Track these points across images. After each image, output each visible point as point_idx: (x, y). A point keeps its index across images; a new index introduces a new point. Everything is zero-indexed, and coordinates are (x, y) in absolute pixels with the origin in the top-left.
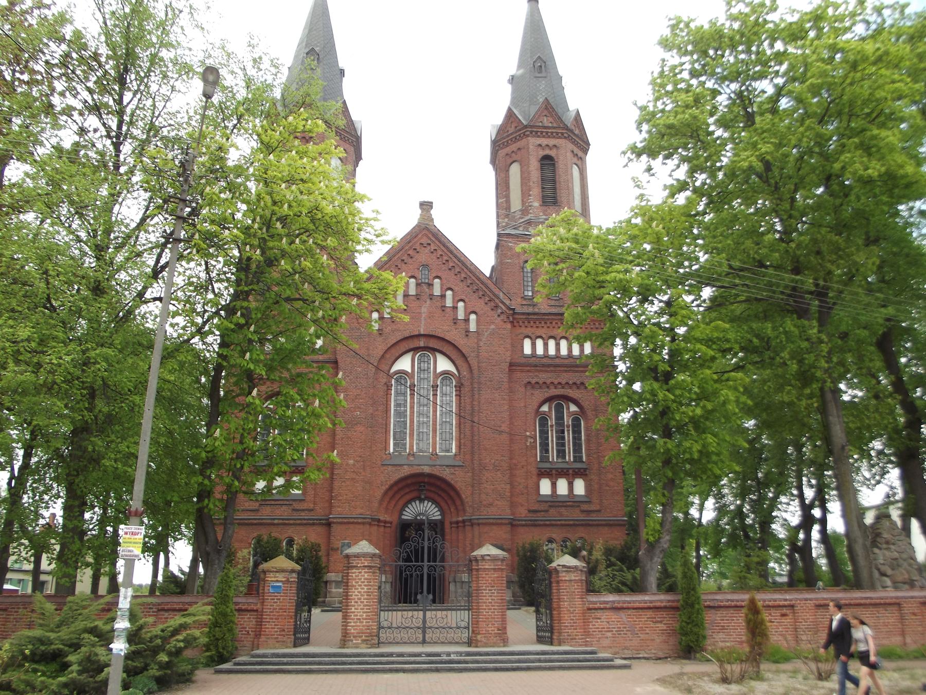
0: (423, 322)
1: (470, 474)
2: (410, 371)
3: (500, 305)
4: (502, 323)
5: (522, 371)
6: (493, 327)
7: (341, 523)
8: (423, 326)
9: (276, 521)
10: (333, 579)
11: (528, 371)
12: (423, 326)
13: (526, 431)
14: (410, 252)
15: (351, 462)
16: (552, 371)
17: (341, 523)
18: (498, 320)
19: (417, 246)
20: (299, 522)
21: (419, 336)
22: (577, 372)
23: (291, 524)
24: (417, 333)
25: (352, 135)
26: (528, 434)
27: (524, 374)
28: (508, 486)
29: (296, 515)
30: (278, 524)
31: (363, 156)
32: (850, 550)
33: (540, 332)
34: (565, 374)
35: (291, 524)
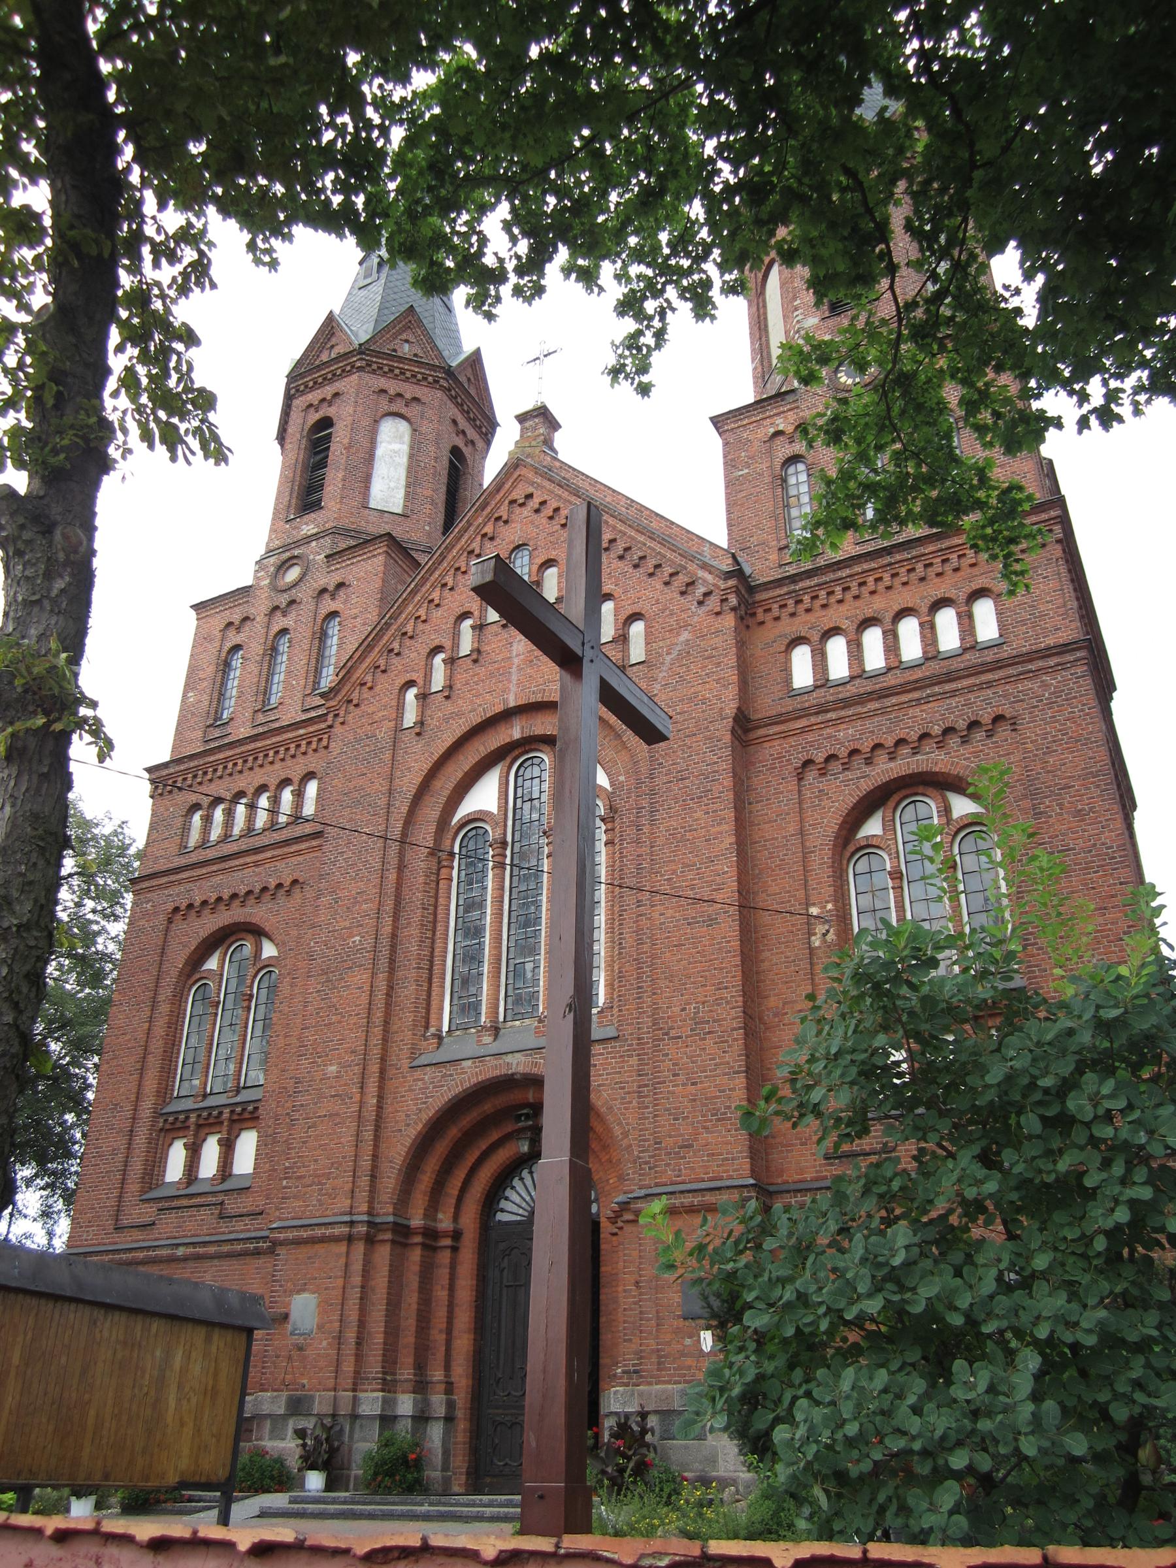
0: (514, 678)
1: (634, 1061)
2: (495, 810)
3: (700, 573)
4: (712, 619)
5: (785, 735)
6: (685, 636)
7: (298, 1242)
8: (513, 688)
9: (180, 1252)
10: (266, 1409)
11: (803, 731)
12: (513, 688)
13: (808, 905)
14: (488, 529)
15: (333, 1069)
16: (875, 713)
17: (298, 1242)
18: (700, 616)
19: (503, 512)
20: (226, 1248)
21: (506, 715)
22: (953, 693)
23: (212, 1257)
24: (499, 708)
25: (433, 367)
26: (814, 911)
27: (792, 741)
28: (740, 1081)
29: (227, 1230)
30: (185, 1259)
31: (499, 419)
32: (197, 1543)
33: (836, 615)
34: (916, 711)
35: (212, 1257)
